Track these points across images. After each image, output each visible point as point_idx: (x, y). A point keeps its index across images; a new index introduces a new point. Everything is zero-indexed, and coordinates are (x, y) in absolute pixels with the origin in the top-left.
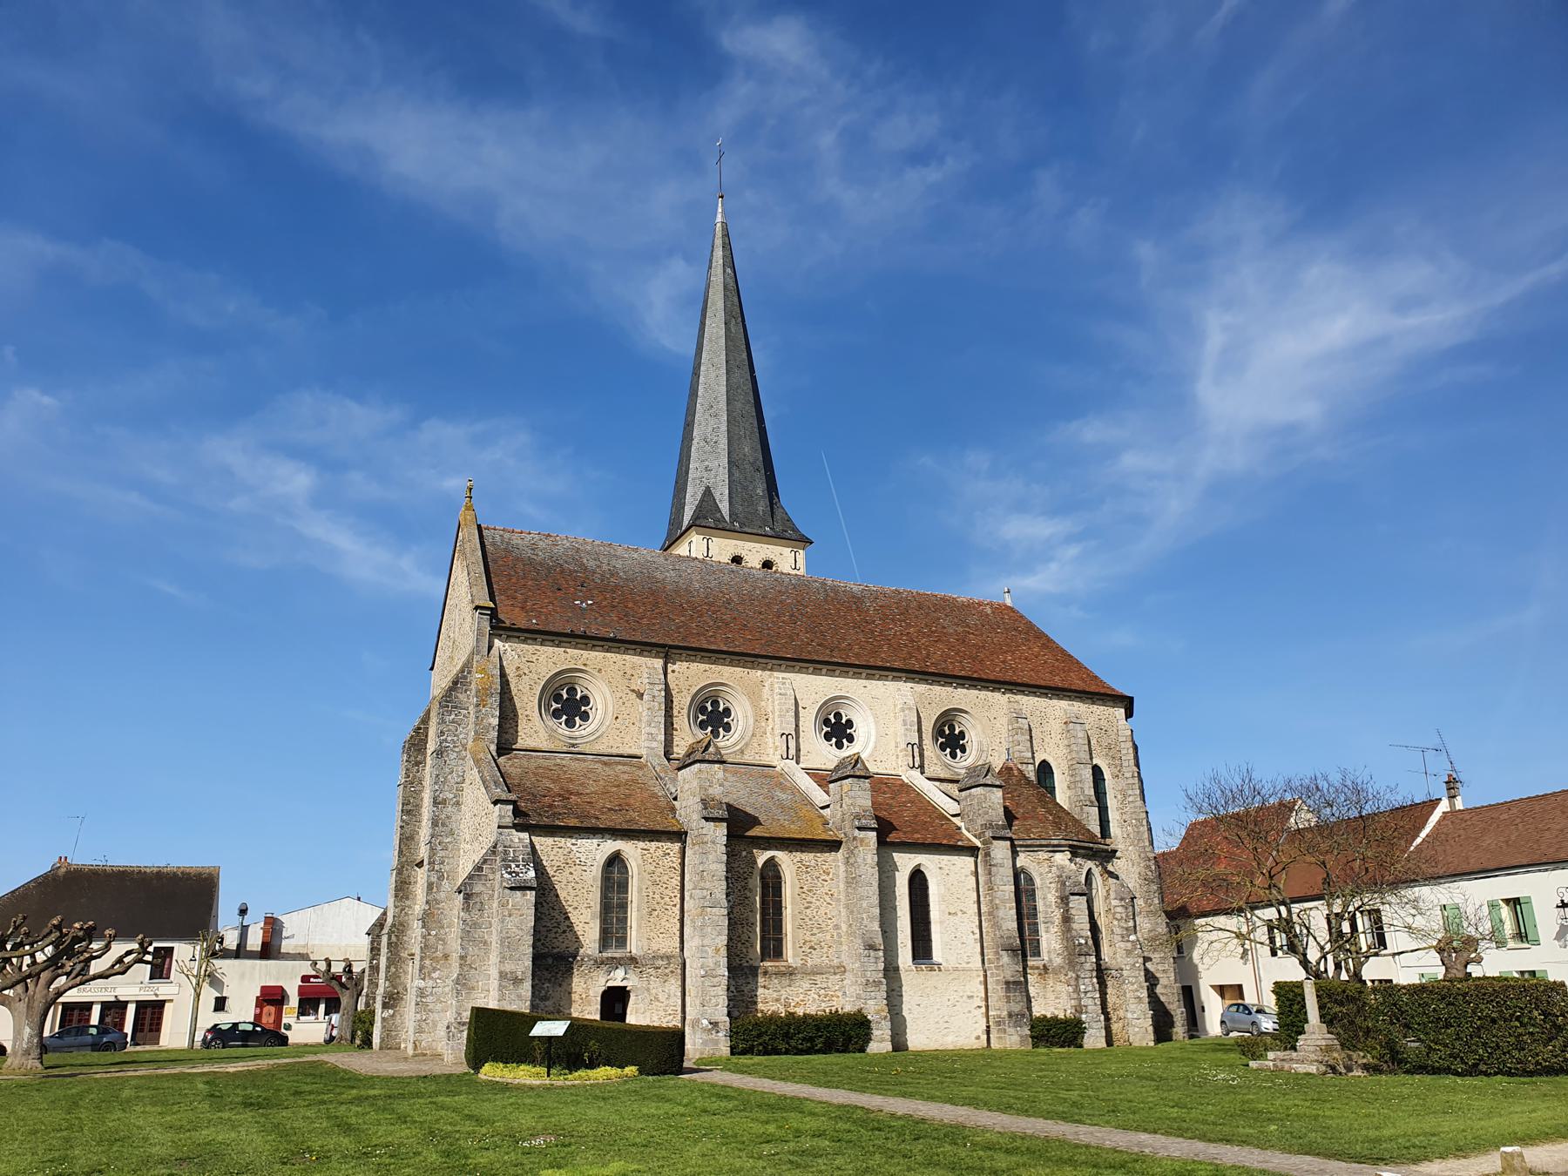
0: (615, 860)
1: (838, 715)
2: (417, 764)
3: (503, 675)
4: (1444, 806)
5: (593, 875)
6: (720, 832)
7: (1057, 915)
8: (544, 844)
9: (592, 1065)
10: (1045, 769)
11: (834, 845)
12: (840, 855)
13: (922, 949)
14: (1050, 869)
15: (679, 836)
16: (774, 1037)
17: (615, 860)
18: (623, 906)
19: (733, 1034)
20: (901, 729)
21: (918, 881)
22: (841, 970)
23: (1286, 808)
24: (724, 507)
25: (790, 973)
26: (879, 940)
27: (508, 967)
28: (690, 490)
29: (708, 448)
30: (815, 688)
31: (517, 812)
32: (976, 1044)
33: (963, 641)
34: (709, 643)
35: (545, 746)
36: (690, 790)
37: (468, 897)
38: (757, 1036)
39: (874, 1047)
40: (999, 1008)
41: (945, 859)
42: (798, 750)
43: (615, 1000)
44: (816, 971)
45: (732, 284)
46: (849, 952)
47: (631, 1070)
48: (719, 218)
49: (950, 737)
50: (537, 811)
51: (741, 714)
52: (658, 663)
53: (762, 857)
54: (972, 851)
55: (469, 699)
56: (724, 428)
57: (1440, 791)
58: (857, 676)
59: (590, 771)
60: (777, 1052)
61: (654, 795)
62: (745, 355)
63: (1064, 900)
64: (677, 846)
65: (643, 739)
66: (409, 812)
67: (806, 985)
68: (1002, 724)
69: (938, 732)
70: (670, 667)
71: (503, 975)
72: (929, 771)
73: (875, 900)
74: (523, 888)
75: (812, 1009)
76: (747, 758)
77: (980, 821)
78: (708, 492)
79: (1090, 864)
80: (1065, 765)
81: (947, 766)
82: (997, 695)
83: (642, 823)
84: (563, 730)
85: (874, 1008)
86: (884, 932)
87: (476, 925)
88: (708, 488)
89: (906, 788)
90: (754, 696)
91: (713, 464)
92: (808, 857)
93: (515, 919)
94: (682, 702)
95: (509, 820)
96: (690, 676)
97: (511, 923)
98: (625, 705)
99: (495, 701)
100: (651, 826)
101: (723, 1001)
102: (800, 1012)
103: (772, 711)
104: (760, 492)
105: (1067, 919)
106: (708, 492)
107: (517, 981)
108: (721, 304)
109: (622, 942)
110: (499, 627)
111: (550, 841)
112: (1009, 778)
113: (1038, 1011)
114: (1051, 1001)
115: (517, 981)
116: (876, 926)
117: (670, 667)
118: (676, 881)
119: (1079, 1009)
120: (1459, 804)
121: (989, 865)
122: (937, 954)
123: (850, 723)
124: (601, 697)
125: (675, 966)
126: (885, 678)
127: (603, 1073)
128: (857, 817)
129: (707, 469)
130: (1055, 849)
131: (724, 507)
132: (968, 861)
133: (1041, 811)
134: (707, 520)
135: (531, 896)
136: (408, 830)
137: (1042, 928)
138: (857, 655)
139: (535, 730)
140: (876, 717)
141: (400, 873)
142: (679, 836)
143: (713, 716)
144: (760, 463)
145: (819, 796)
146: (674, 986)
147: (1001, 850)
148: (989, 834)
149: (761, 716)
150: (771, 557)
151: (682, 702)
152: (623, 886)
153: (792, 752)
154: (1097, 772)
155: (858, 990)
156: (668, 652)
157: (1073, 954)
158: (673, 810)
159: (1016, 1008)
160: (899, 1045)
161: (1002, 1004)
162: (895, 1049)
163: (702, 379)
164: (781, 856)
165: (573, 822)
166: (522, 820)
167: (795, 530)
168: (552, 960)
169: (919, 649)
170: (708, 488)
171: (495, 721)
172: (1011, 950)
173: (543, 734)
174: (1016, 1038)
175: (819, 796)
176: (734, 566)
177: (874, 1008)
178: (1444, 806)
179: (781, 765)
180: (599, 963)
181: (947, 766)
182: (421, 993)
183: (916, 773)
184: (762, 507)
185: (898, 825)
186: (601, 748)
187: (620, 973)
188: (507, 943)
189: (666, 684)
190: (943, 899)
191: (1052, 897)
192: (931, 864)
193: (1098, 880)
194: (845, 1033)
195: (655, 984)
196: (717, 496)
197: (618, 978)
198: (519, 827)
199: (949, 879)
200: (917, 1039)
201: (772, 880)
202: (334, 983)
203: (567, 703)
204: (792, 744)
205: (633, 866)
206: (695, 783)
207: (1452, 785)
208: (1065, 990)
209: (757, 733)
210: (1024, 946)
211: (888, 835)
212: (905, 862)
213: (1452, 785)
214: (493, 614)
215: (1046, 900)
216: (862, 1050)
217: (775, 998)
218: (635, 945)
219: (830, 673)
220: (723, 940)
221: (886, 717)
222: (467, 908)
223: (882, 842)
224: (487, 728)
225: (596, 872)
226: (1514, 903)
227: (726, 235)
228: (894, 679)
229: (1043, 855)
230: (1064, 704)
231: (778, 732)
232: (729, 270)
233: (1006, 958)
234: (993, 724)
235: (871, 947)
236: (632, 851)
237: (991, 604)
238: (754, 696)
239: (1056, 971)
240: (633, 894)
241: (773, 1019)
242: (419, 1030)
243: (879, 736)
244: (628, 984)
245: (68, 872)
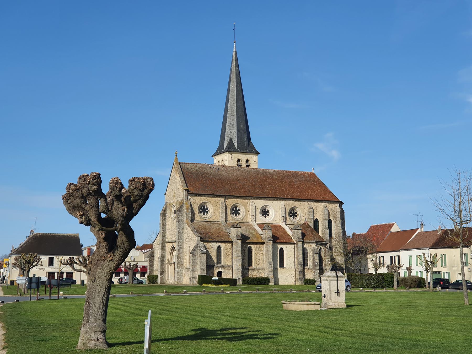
0: (219, 247)
1: (265, 209)
2: (165, 219)
3: (191, 204)
4: (419, 230)
5: (215, 249)
6: (240, 242)
7: (312, 258)
8: (206, 244)
9: (222, 284)
10: (316, 222)
11: (263, 243)
12: (265, 245)
13: (282, 264)
14: (311, 248)
15: (231, 242)
16: (250, 281)
17: (219, 247)
18: (221, 256)
19: (243, 280)
20: (281, 213)
21: (282, 250)
22: (264, 269)
23: (391, 225)
24: (236, 145)
25: (254, 269)
26: (272, 263)
27: (202, 268)
28: (226, 138)
29: (231, 126)
30: (260, 203)
31: (201, 238)
32: (292, 284)
33: (298, 187)
34: (235, 194)
35: (199, 220)
36: (234, 233)
37: (193, 254)
38: (247, 281)
39: (270, 284)
40: (298, 277)
41: (288, 246)
42: (256, 219)
43: (220, 274)
44: (259, 269)
45: (238, 73)
46: (266, 265)
47: (228, 285)
48: (234, 50)
49: (293, 214)
50: (204, 237)
51: (242, 210)
52: (223, 199)
53: (249, 246)
54: (294, 244)
55: (184, 210)
56: (236, 120)
57: (419, 227)
58: (270, 200)
59: (210, 226)
60: (251, 284)
61: (225, 232)
62: (241, 96)
63: (313, 254)
64: (231, 244)
65: (220, 218)
66: (163, 231)
67: (257, 272)
68: (306, 210)
69: (290, 212)
70: (226, 200)
71: (201, 269)
72: (288, 222)
73: (272, 255)
74: (204, 253)
75: (258, 276)
76: (244, 221)
77: (296, 237)
78: (231, 140)
79: (321, 246)
80: (322, 219)
81: (292, 221)
82: (306, 203)
83: (224, 240)
84: (203, 216)
85: (271, 276)
86: (273, 261)
87: (195, 260)
88: (231, 138)
89: (281, 227)
90: (245, 206)
91: (233, 131)
92: (258, 246)
93: (203, 259)
94: (229, 208)
95: (199, 240)
96: (231, 202)
97: (202, 260)
98: (216, 209)
99: (190, 211)
100: (225, 240)
101: (241, 275)
102: (255, 277)
103: (249, 209)
104: (245, 139)
105: (314, 259)
106: (231, 140)
107: (204, 270)
108: (235, 80)
109: (221, 263)
110: (189, 193)
111: (207, 243)
112: (305, 225)
113: (307, 277)
114: (309, 276)
115: (204, 270)
116: (272, 260)
117: (226, 200)
118: (231, 251)
119: (315, 278)
120: (423, 230)
121: (297, 247)
122: (285, 266)
123: (268, 211)
124: (211, 209)
125: (231, 268)
126: (278, 200)
127: (224, 285)
128: (269, 238)
129: (231, 132)
130: (313, 243)
131: (236, 145)
132: (293, 246)
133: (311, 234)
134: (231, 149)
135: (205, 255)
136: (163, 235)
137: (308, 260)
138: (271, 194)
139: (198, 217)
140: (274, 210)
141: (162, 244)
142: (231, 242)
143: (235, 211)
144: (245, 130)
145: (260, 231)
146: (231, 271)
147: (300, 244)
148: (298, 240)
149: (247, 211)
150: (248, 158)
151: (229, 208)
152: (221, 252)
153: (254, 219)
154: (330, 222)
155: (267, 273)
156: (226, 197)
157: (315, 266)
158: (229, 236)
159: (301, 277)
160: (276, 283)
161: (298, 276)
162: (275, 284)
163: (229, 104)
164: (252, 246)
165: (211, 240)
166: (202, 239)
167: (255, 149)
168: (210, 266)
169: (287, 191)
170: (231, 138)
171: (190, 215)
172: (301, 265)
173: (199, 217)
174: (300, 283)
175: (260, 231)
176: (239, 168)
177: (271, 276)
178: (419, 230)
179: (251, 223)
180: (217, 267)
181: (292, 221)
182: (178, 272)
183: (284, 223)
184: (246, 144)
185: (278, 238)
186: (211, 220)
187: (221, 269)
188: (202, 264)
189: (225, 205)
190: (287, 254)
191: (311, 254)
192: (284, 247)
193: (323, 250)
194: (264, 281)
195: (227, 271)
196: (233, 140)
197: (220, 270)
198: (202, 241)
199: (288, 250)
200: (281, 283)
201: (250, 251)
202: (127, 268)
203: (203, 209)
204: (254, 218)
205: (222, 248)
206: (235, 232)
207: (422, 225)
208: (312, 273)
209: (246, 215)
210: (304, 264)
211: (275, 239)
212: (280, 246)
213: (422, 225)
214: (188, 191)
215: (310, 254)
216: (268, 284)
217: (253, 274)
218: (223, 263)
219: (264, 200)
220: (241, 263)
221: (276, 210)
222: (193, 257)
223: (274, 242)
224: (188, 217)
225: (215, 249)
226: (445, 255)
227: (236, 56)
228: (280, 200)
229: (310, 245)
230: (323, 204)
231: (251, 215)
232: (237, 68)
233: (299, 267)
234: (304, 211)
235: (270, 264)
236: (222, 245)
237: (308, 173)
238: (245, 206)
239: (311, 269)
240: (223, 254)
241: (251, 278)
242: (178, 279)
243: (275, 215)
244: (222, 271)
245: (40, 235)
